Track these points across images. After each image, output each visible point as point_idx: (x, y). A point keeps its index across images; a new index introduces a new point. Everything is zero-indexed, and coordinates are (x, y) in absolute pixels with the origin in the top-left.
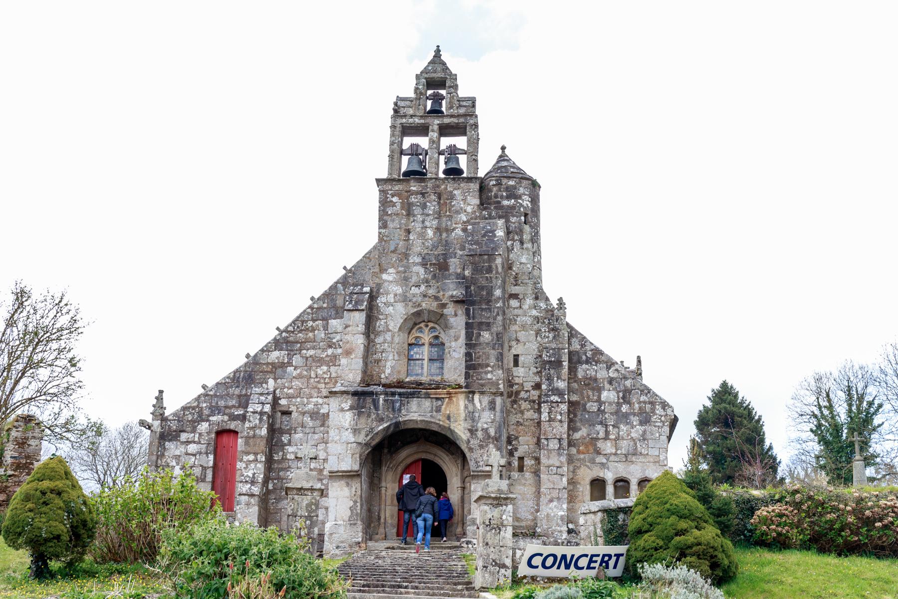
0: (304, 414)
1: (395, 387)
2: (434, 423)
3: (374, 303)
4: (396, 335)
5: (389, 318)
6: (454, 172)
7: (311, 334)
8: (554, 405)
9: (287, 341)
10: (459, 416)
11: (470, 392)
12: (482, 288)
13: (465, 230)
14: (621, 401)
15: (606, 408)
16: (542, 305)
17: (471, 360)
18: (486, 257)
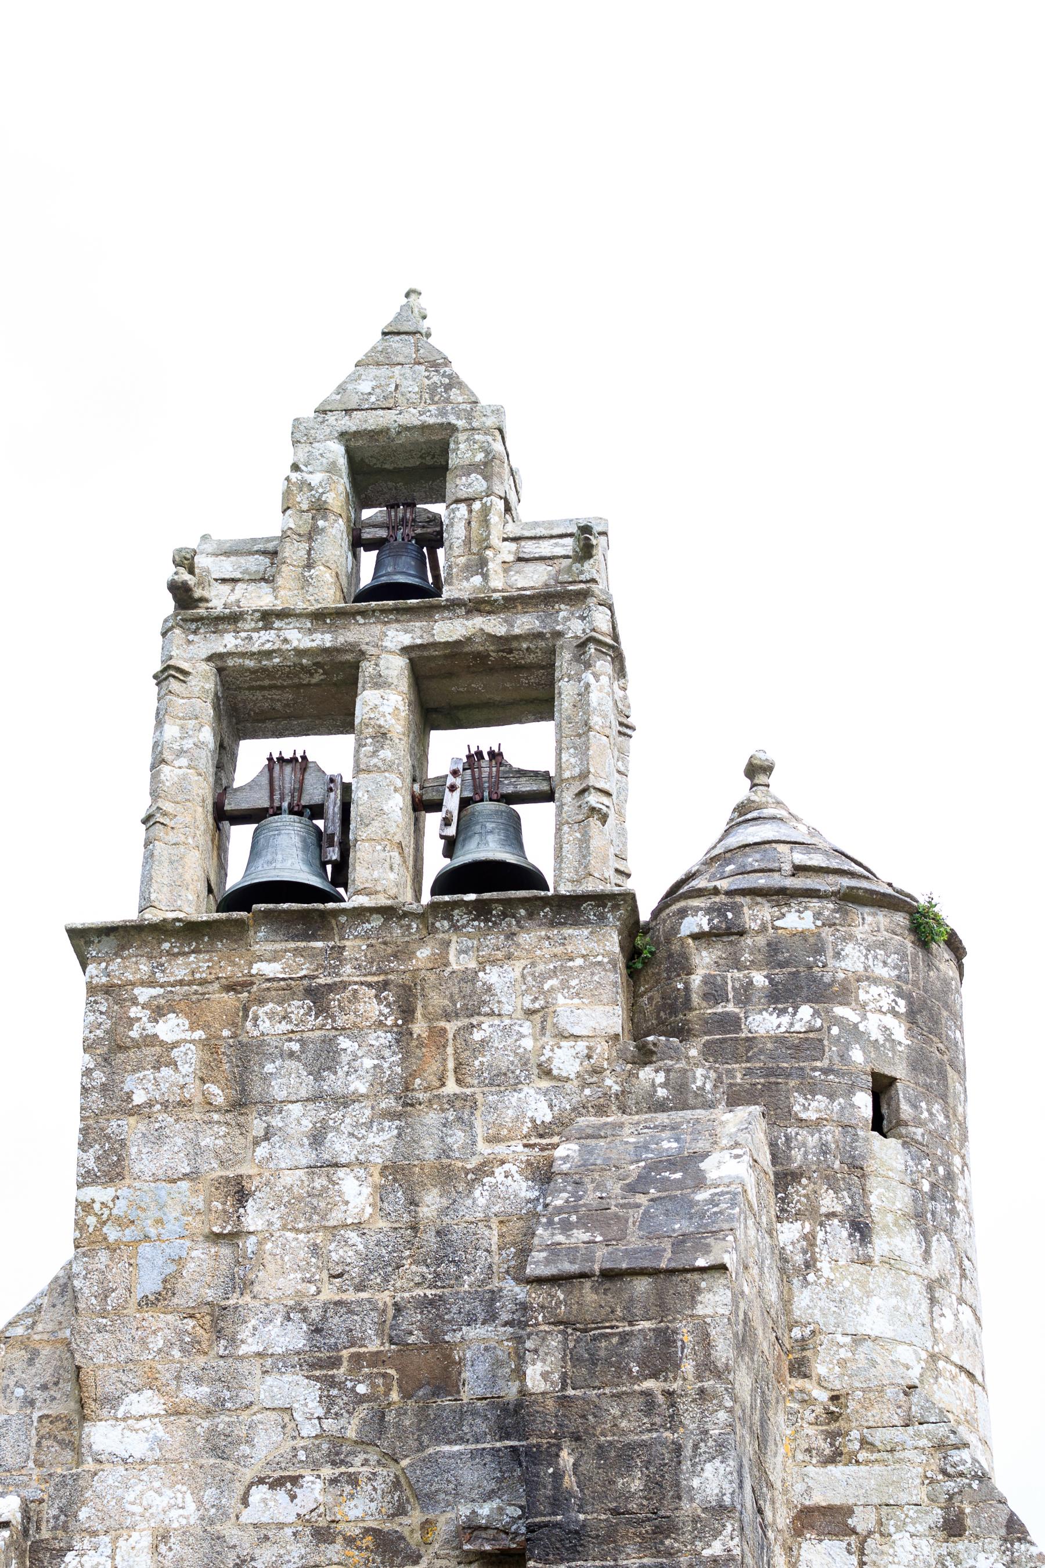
6: (490, 888)
12: (624, 1456)
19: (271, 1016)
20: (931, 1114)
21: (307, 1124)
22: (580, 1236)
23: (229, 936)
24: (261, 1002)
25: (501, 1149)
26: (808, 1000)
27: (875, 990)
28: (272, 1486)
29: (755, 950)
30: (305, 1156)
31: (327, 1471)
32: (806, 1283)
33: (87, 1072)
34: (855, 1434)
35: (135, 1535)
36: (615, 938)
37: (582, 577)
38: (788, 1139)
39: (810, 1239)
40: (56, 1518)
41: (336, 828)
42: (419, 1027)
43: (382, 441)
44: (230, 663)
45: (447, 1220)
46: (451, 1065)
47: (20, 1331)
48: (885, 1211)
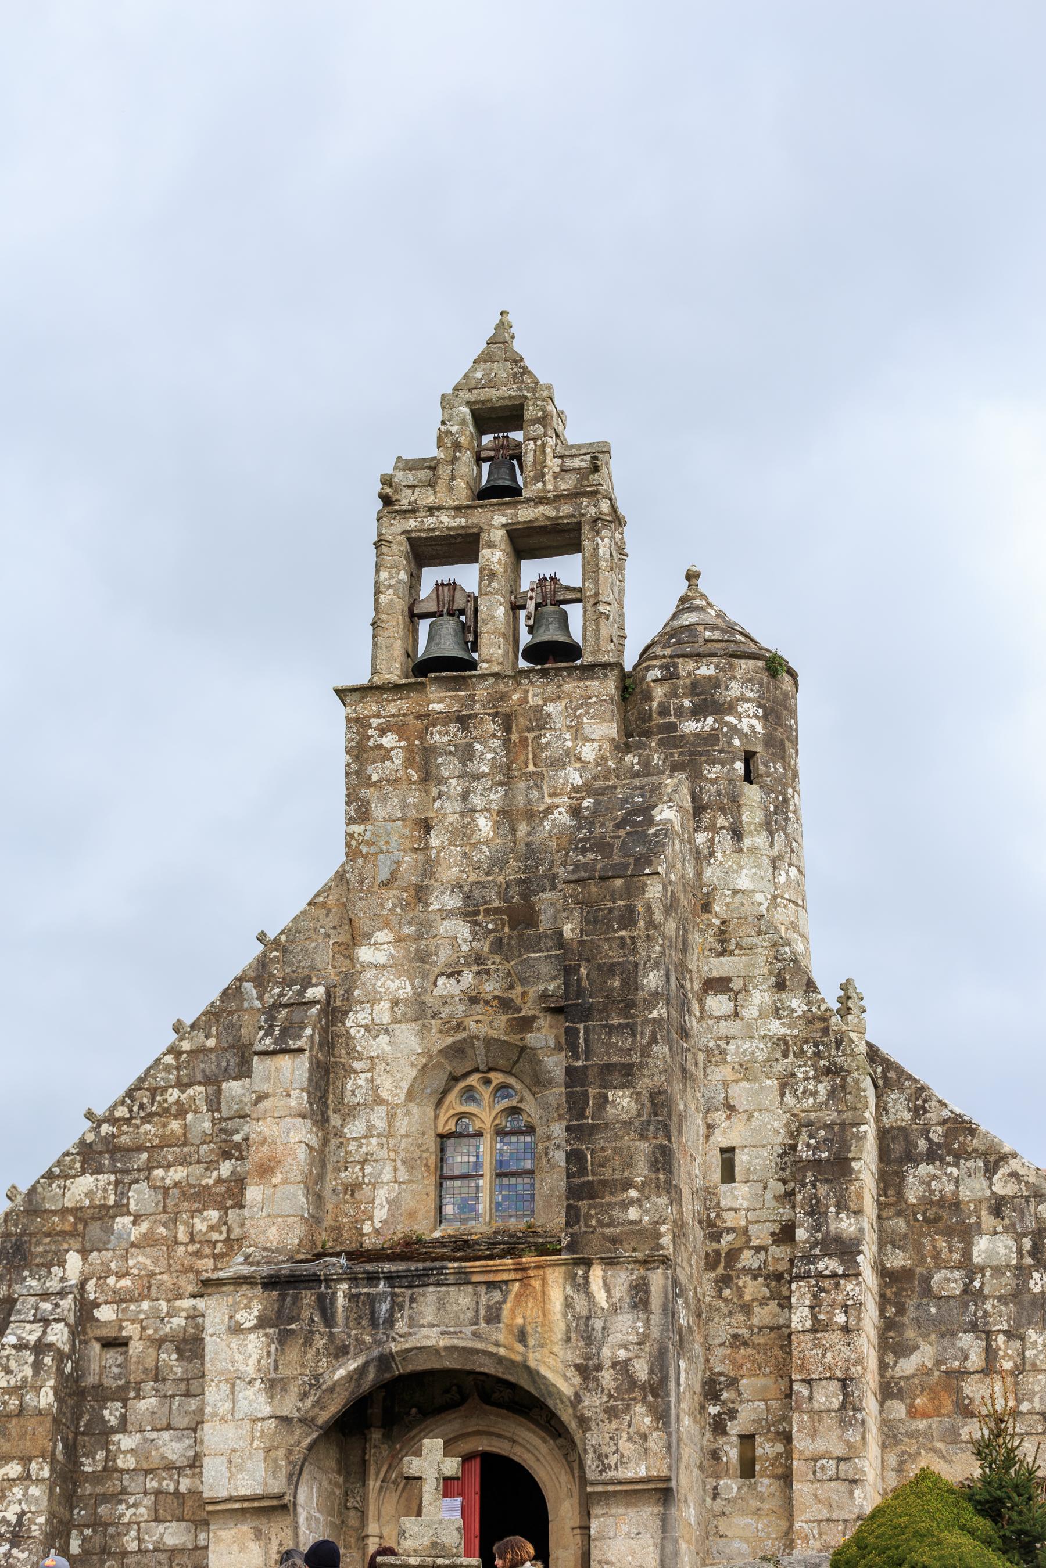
0: (159, 1343)
1: (392, 1258)
2: (485, 1352)
3: (339, 1028)
4: (400, 1112)
5: (380, 1067)
6: (553, 655)
7: (175, 1125)
8: (826, 1284)
9: (112, 1147)
10: (551, 1325)
11: (577, 1262)
12: (611, 969)
13: (575, 811)
14: (1029, 1261)
15: (991, 1285)
16: (794, 1004)
17: (583, 1171)
18: (619, 883)
19: (440, 732)
20: (776, 769)
21: (459, 790)
22: (591, 856)
23: (417, 690)
24: (434, 726)
25: (556, 800)
26: (711, 714)
27: (746, 706)
28: (448, 976)
29: (684, 687)
30: (458, 806)
31: (475, 968)
32: (709, 864)
33: (348, 765)
34: (733, 941)
35: (382, 1003)
36: (612, 685)
37: (595, 483)
38: (701, 788)
39: (712, 841)
40: (343, 995)
41: (471, 623)
42: (514, 737)
43: (489, 405)
44: (413, 535)
45: (530, 838)
46: (531, 756)
47: (321, 899)
48: (749, 824)
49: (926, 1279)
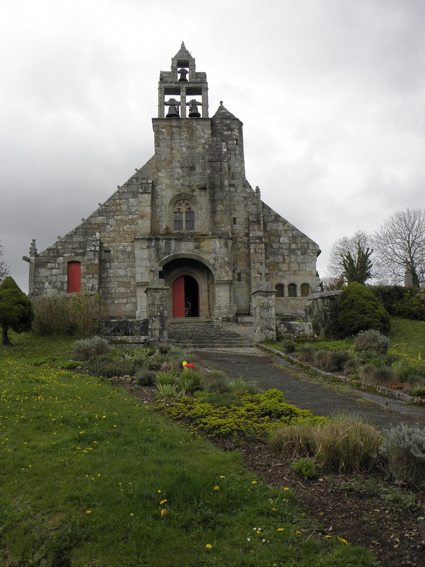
4: (168, 207)
7: (119, 207)
8: (258, 244)
49: (271, 245)
